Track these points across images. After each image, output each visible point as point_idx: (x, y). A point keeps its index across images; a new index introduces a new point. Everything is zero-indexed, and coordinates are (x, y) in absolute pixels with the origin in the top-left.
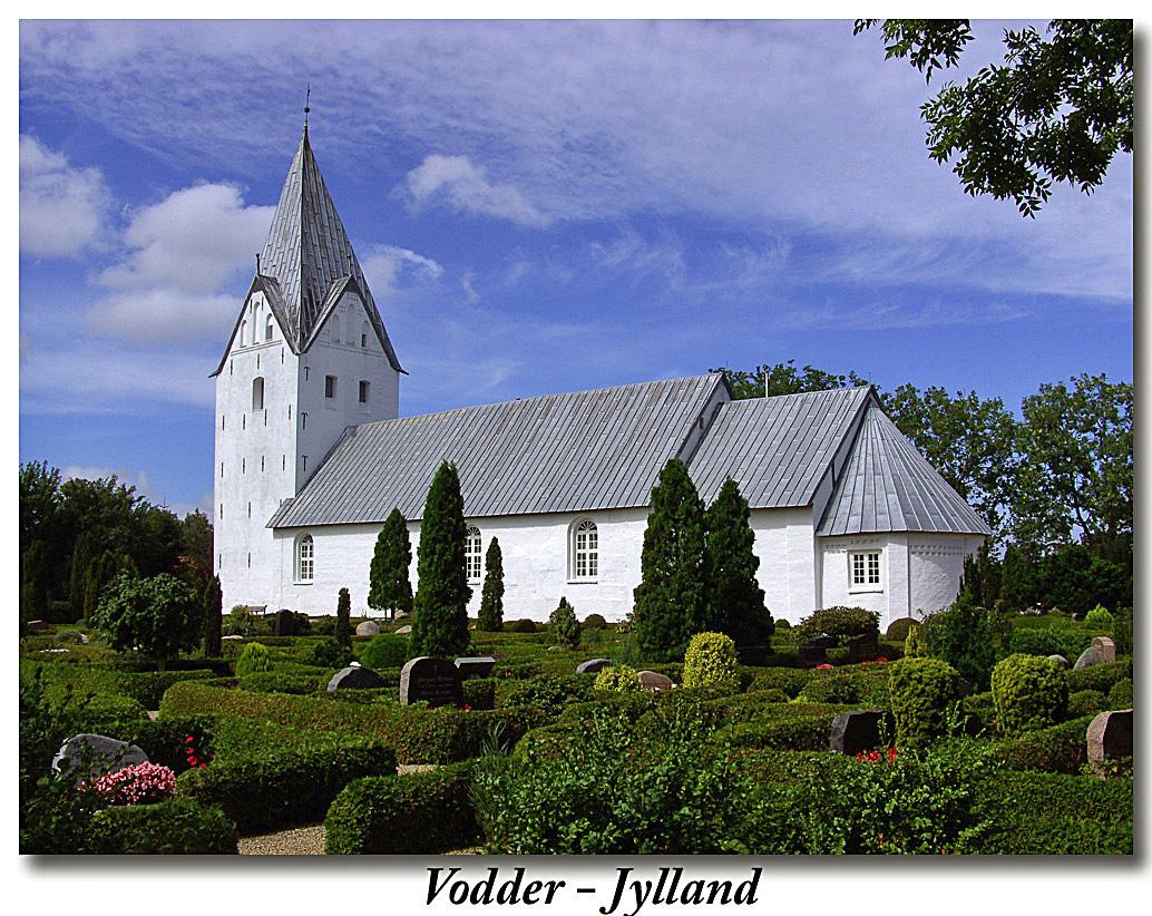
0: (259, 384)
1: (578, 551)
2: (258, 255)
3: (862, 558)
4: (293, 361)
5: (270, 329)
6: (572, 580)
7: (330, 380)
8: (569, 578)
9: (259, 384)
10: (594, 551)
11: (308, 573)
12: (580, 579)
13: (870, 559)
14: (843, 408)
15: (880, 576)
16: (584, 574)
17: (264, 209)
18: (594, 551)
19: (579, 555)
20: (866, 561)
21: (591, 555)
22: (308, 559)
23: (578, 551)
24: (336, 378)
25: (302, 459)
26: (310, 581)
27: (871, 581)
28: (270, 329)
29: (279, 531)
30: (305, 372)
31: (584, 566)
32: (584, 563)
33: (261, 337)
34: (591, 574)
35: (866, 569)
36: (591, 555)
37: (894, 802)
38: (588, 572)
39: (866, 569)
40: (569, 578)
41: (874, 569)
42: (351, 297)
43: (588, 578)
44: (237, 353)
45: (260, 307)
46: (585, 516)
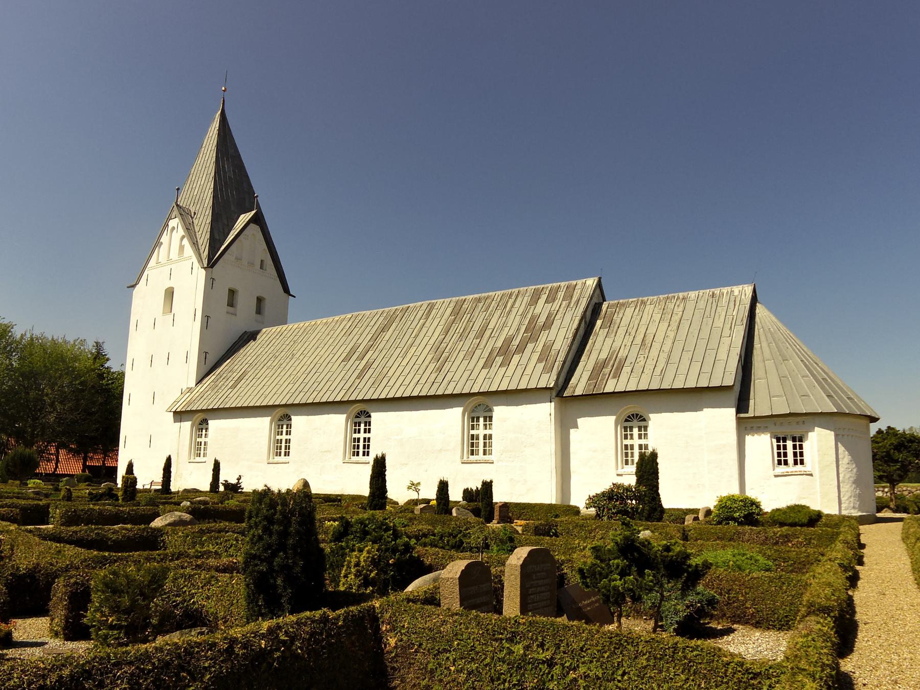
1: (472, 432)
2: (178, 189)
4: (201, 274)
5: (182, 248)
6: (192, 460)
7: (232, 293)
10: (367, 435)
11: (283, 451)
13: (485, 421)
14: (404, 333)
15: (805, 458)
16: (358, 455)
18: (367, 435)
19: (355, 439)
20: (789, 444)
21: (286, 440)
22: (362, 435)
23: (472, 432)
25: (203, 354)
26: (286, 459)
27: (796, 463)
28: (182, 248)
29: (180, 415)
30: (210, 283)
31: (281, 449)
32: (281, 447)
34: (364, 455)
35: (790, 451)
37: (694, 667)
38: (283, 454)
39: (790, 451)
40: (462, 457)
42: (254, 228)
45: (175, 231)
46: (480, 399)
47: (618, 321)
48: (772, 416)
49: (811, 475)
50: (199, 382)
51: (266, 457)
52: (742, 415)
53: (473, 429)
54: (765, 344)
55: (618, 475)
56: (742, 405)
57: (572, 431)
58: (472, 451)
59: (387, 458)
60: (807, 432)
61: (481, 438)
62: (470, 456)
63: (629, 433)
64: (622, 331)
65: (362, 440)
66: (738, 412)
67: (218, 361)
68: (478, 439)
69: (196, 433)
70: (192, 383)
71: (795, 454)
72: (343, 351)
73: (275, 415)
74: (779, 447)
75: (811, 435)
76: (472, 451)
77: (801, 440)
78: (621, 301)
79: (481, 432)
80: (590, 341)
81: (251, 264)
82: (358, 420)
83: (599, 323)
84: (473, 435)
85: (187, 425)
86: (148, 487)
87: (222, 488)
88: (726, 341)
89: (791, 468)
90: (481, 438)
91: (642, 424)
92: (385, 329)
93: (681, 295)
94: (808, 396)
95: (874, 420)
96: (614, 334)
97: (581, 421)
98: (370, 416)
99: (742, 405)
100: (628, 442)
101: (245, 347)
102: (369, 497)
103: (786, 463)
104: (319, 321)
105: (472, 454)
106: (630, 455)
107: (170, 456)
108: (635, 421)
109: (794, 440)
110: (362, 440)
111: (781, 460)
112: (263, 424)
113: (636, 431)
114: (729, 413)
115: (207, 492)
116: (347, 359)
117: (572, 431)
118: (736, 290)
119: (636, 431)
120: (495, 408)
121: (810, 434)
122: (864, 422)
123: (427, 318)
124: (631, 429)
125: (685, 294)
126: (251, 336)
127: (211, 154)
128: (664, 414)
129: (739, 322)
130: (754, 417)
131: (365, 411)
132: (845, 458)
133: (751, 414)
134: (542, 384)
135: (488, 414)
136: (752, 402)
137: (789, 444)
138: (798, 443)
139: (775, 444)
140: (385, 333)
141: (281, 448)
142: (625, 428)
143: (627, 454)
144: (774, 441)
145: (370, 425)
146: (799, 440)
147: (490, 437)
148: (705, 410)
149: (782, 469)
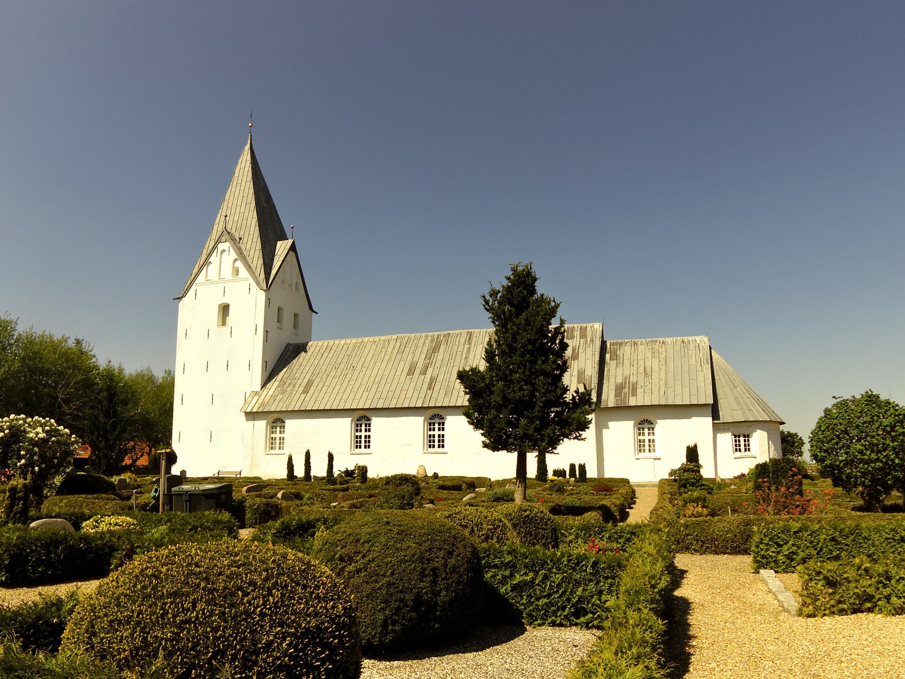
0: (225, 309)
1: (272, 435)
3: (361, 426)
6: (267, 453)
8: (424, 450)
9: (225, 309)
10: (367, 434)
12: (358, 451)
13: (366, 426)
15: (751, 447)
17: (813, 426)
20: (742, 439)
21: (366, 437)
23: (272, 435)
24: (283, 309)
25: (265, 363)
27: (746, 450)
30: (268, 301)
33: (227, 272)
34: (280, 449)
35: (742, 443)
36: (366, 437)
39: (742, 443)
41: (441, 439)
43: (363, 450)
44: (201, 284)
47: (622, 355)
48: (734, 422)
49: (755, 457)
50: (264, 385)
51: (264, 450)
52: (716, 422)
53: (272, 433)
54: (721, 377)
55: (637, 459)
56: (715, 414)
57: (604, 431)
58: (272, 447)
59: (698, 447)
60: (752, 432)
61: (278, 439)
62: (429, 449)
63: (641, 432)
64: (627, 363)
65: (436, 437)
66: (713, 420)
67: (274, 368)
68: (275, 440)
69: (270, 430)
70: (257, 386)
71: (745, 445)
72: (404, 367)
73: (271, 418)
74: (736, 441)
75: (754, 434)
76: (272, 447)
77: (748, 436)
78: (619, 341)
79: (278, 435)
80: (606, 369)
81: (290, 285)
82: (432, 421)
83: (608, 356)
84: (272, 438)
85: (261, 425)
86: (216, 475)
87: (550, 475)
88: (701, 374)
89: (743, 453)
90: (278, 439)
91: (651, 426)
92: (435, 350)
93: (661, 339)
94: (752, 410)
95: (782, 423)
96: (621, 365)
97: (611, 424)
98: (284, 422)
99: (715, 414)
100: (641, 438)
101: (297, 359)
102: (304, 477)
103: (740, 450)
104: (366, 340)
105: (272, 449)
106: (652, 446)
107: (308, 450)
108: (646, 424)
109: (744, 436)
110: (436, 437)
111: (737, 449)
112: (346, 424)
113: (646, 431)
114: (708, 421)
115: (323, 478)
116: (411, 372)
117: (604, 431)
118: (698, 339)
119: (646, 431)
120: (448, 417)
121: (754, 433)
122: (777, 425)
123: (470, 344)
124: (643, 429)
125: (664, 339)
126: (299, 349)
127: (245, 177)
128: (675, 420)
129: (705, 362)
130: (723, 423)
131: (365, 416)
132: (771, 445)
133: (721, 421)
134: (459, 404)
135: (441, 421)
136: (720, 413)
137: (742, 439)
138: (747, 439)
139: (734, 439)
140: (436, 354)
141: (361, 442)
142: (639, 429)
143: (640, 445)
144: (733, 437)
145: (284, 428)
146: (746, 436)
147: (283, 439)
148: (694, 418)
149: (738, 454)
